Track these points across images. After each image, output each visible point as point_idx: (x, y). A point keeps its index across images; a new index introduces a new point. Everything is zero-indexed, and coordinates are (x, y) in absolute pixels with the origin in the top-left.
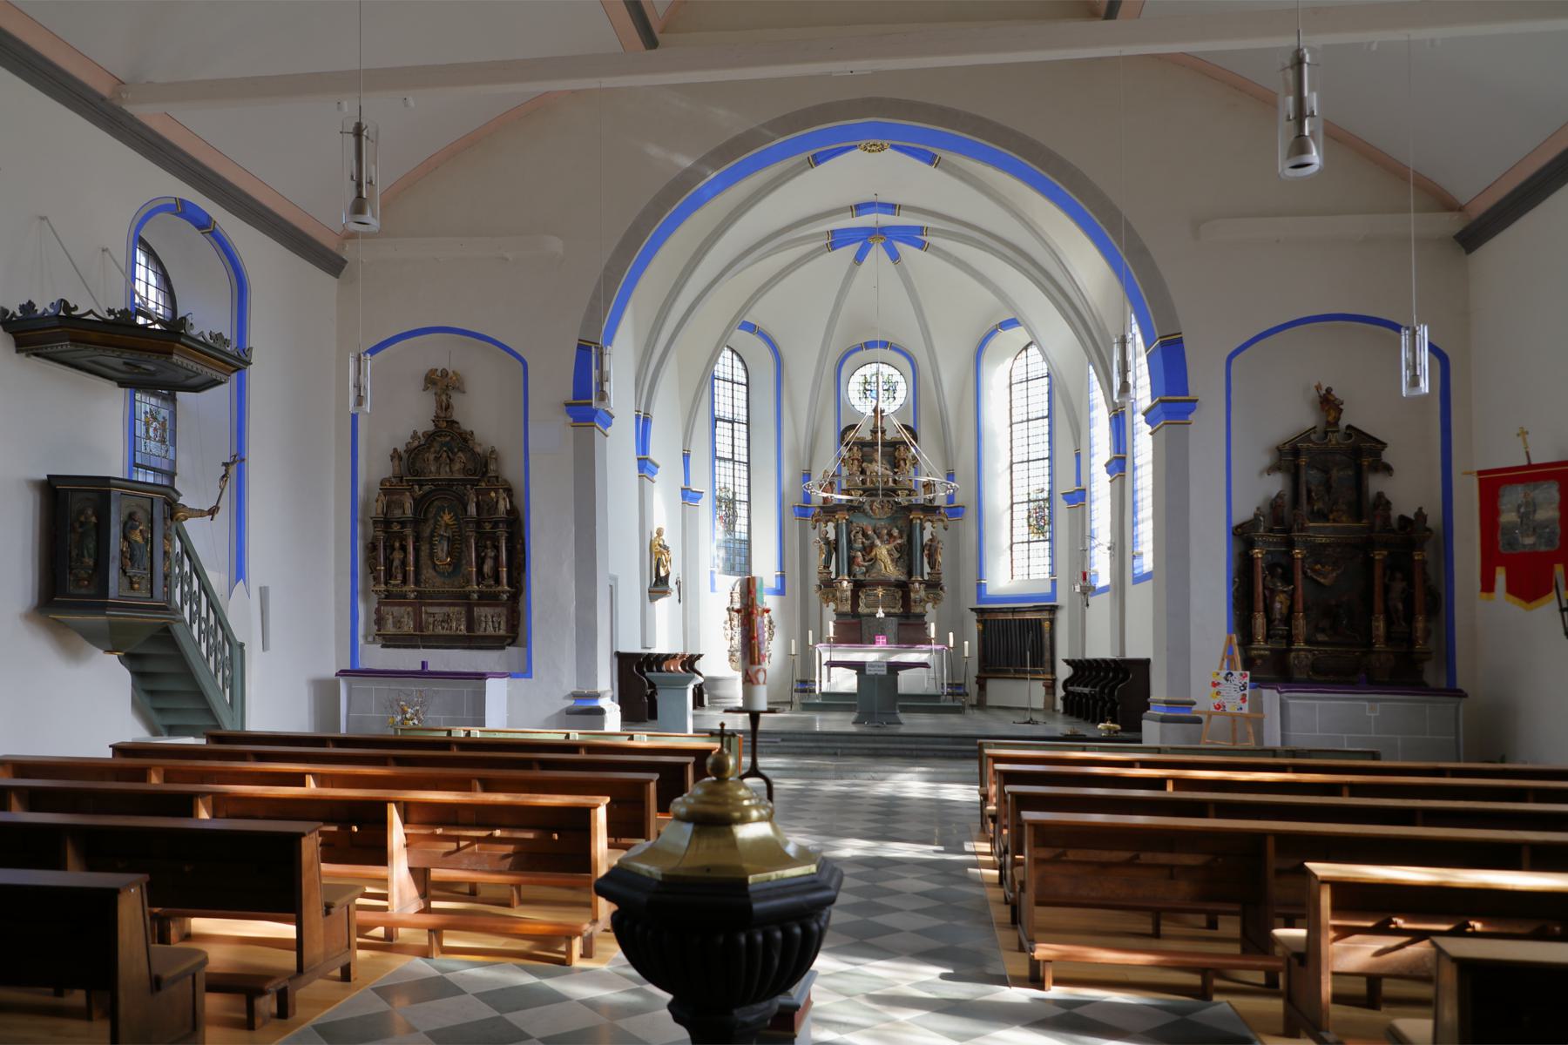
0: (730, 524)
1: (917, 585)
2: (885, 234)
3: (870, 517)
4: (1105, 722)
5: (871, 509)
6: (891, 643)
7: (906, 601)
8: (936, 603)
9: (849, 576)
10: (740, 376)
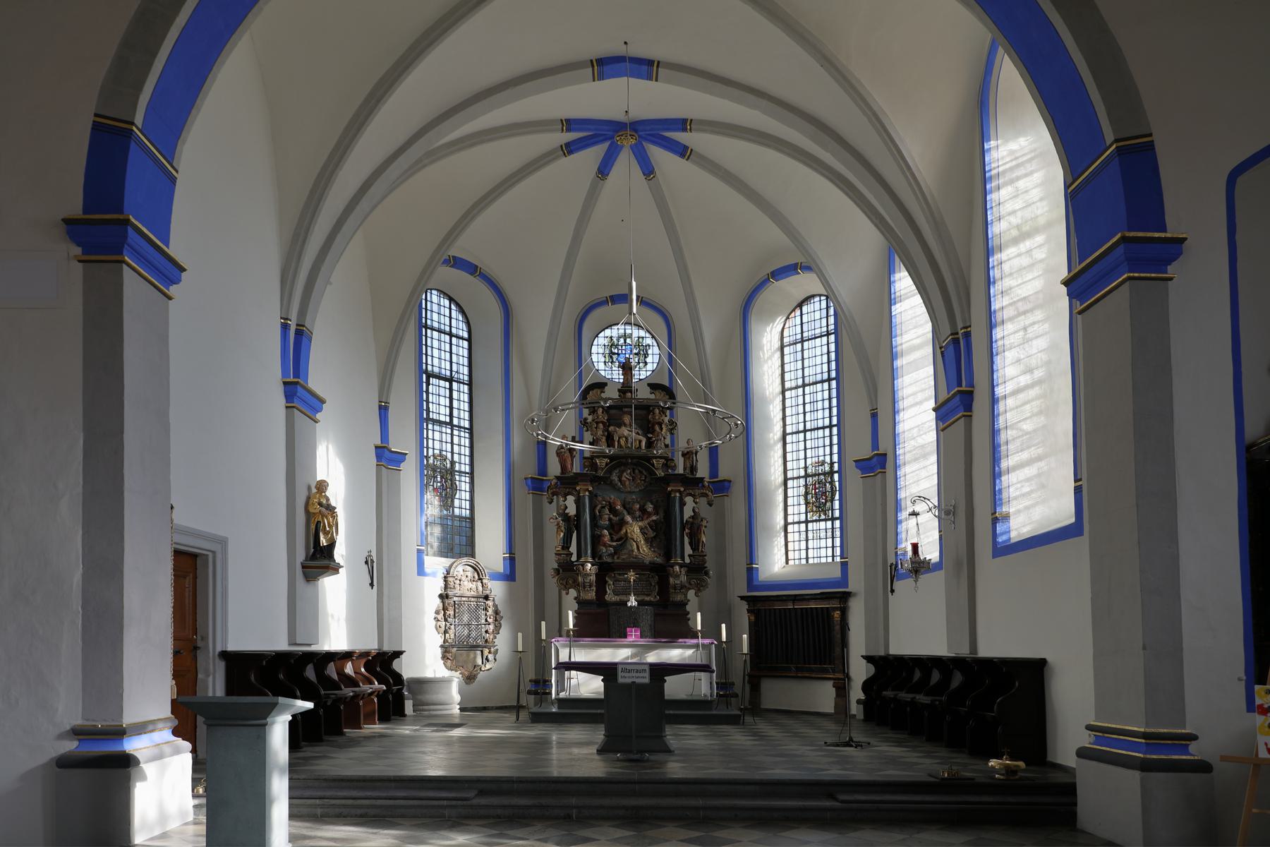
0: (447, 496)
1: (677, 568)
2: (636, 131)
3: (619, 490)
4: (1001, 758)
5: (620, 481)
6: (646, 637)
7: (664, 587)
8: (699, 590)
9: (593, 557)
10: (460, 328)
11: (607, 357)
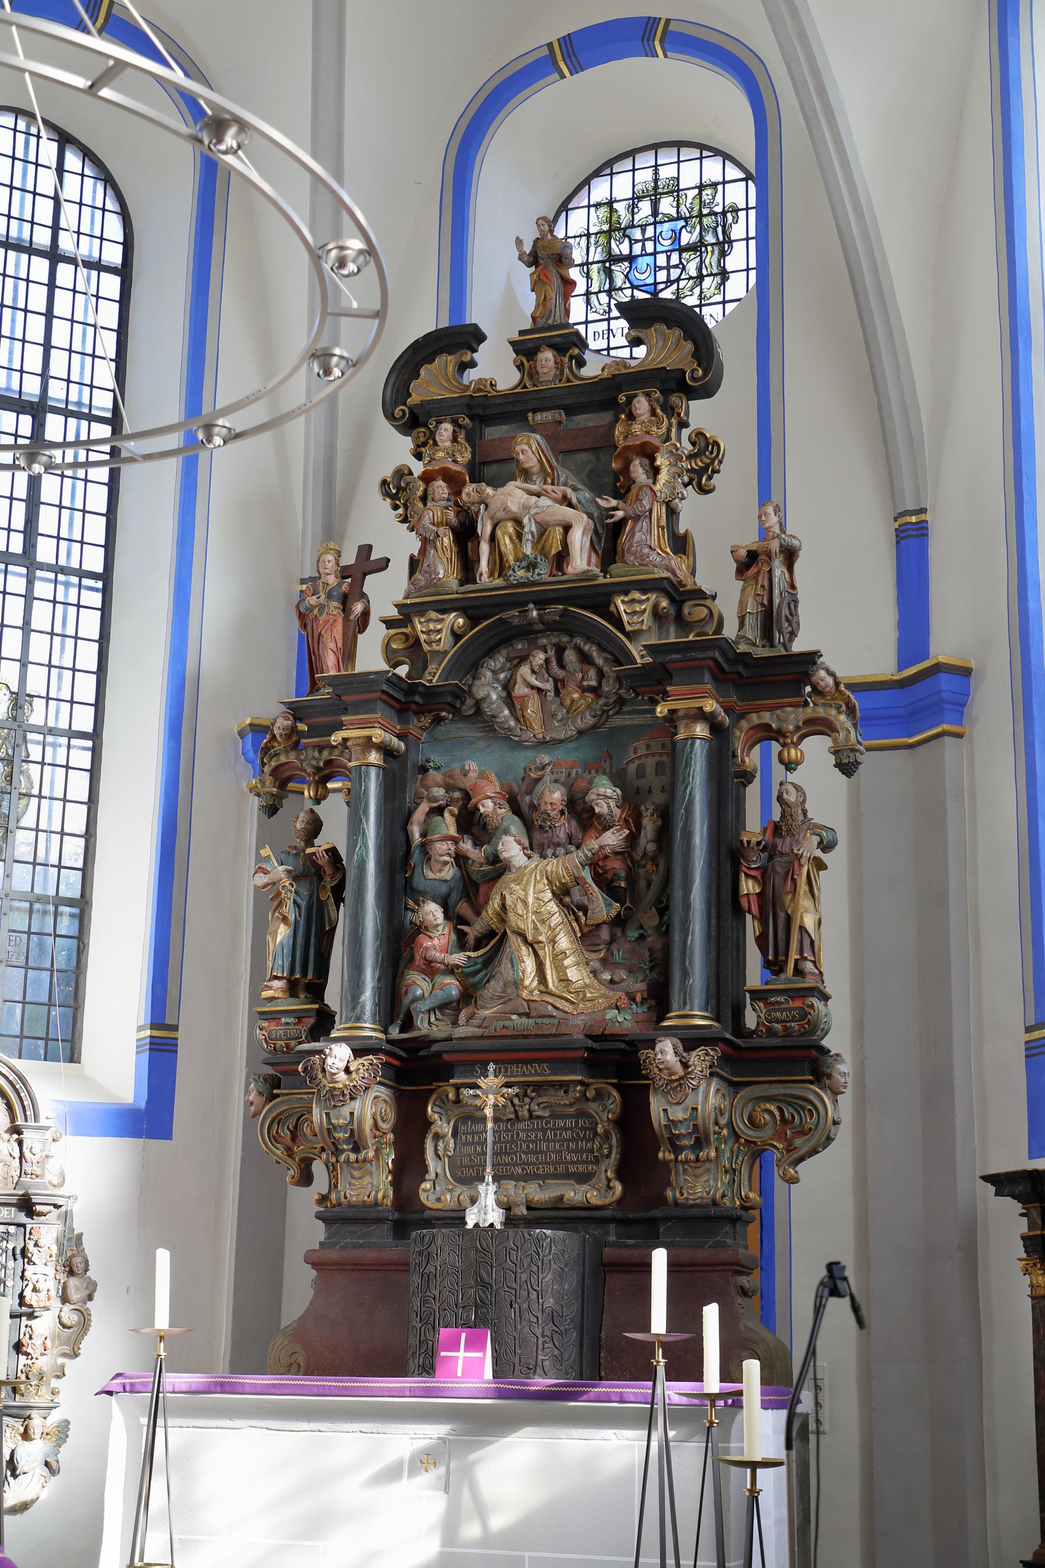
5: (509, 700)
11: (594, 274)
